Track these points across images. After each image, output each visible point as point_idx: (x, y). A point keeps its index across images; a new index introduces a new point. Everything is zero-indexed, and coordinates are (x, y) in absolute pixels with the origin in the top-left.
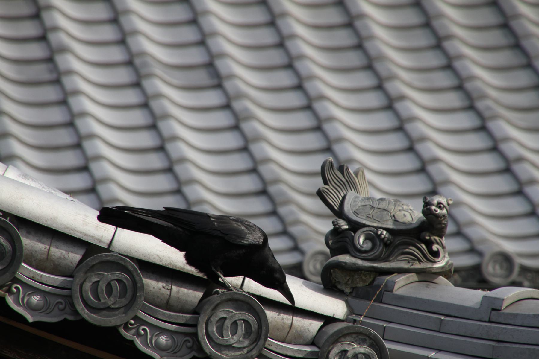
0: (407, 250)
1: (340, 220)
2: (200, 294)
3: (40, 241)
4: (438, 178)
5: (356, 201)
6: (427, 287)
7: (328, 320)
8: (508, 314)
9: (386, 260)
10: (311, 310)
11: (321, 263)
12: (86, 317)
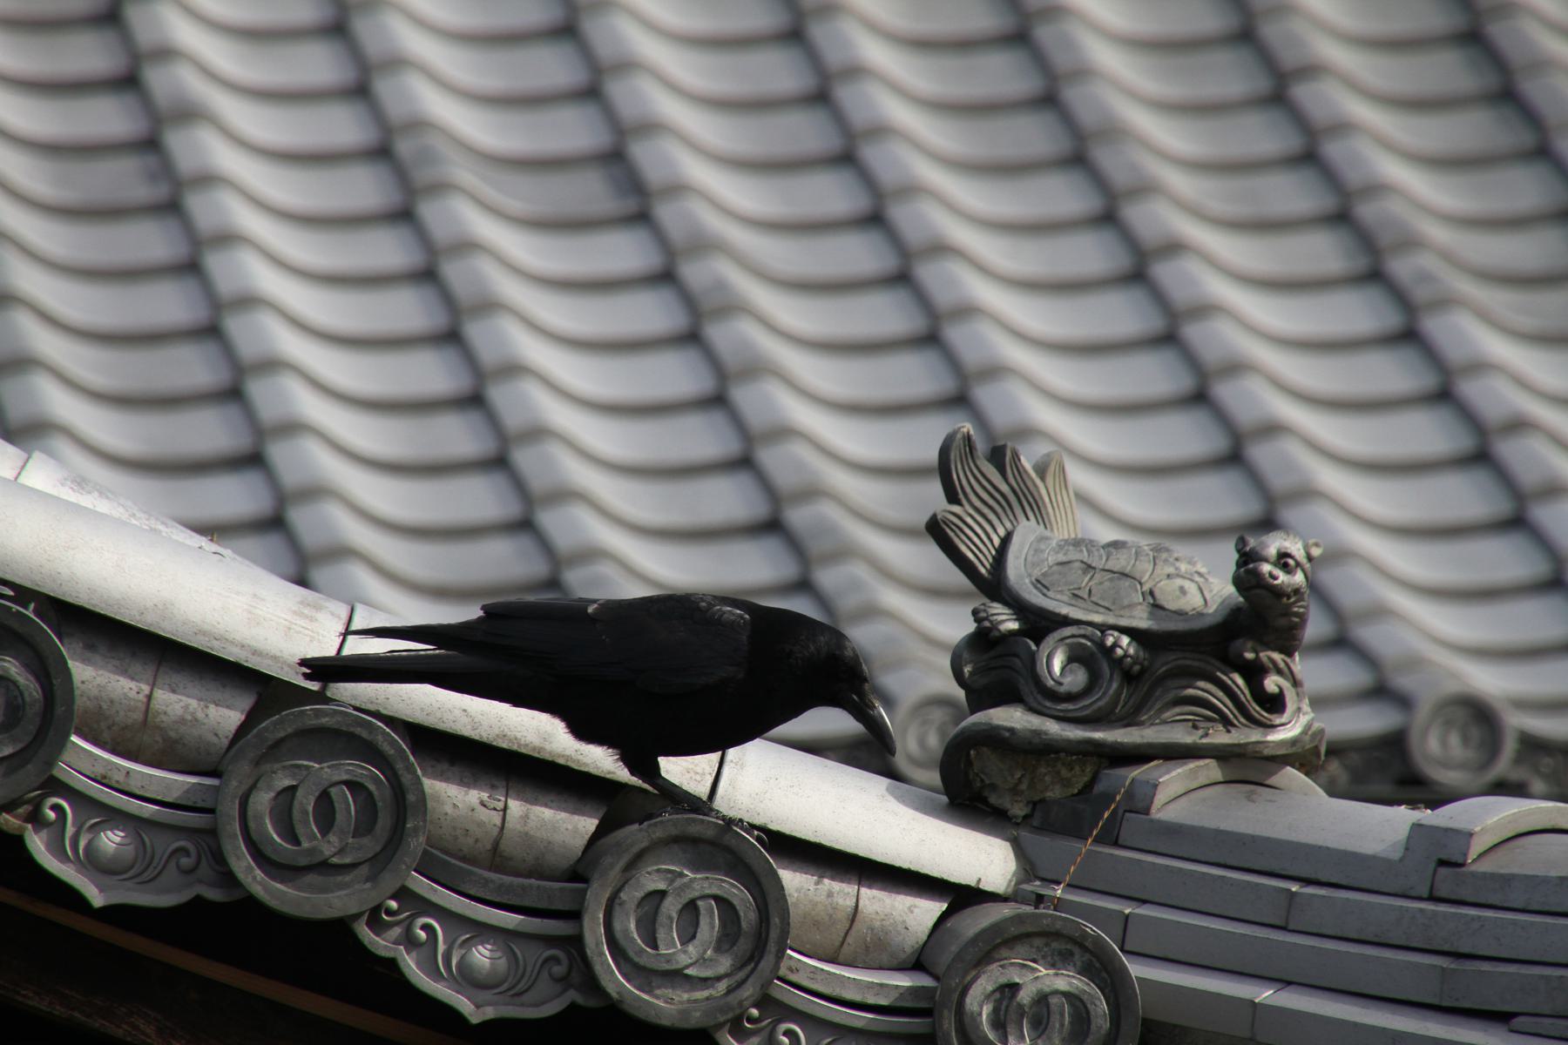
0: (1191, 691)
1: (995, 605)
2: (588, 824)
3: (124, 672)
4: (1279, 481)
7: (961, 897)
9: (1129, 720)
10: (913, 868)
11: (942, 732)
12: (257, 891)
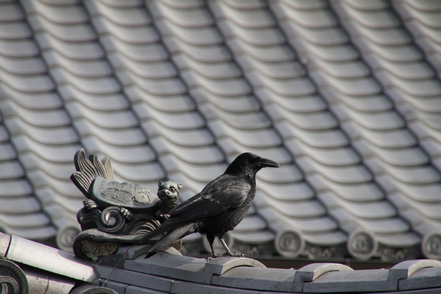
0: (145, 225)
1: (90, 200)
4: (168, 167)
5: (104, 185)
6: (161, 256)
9: (127, 233)
10: (64, 275)
11: (72, 237)
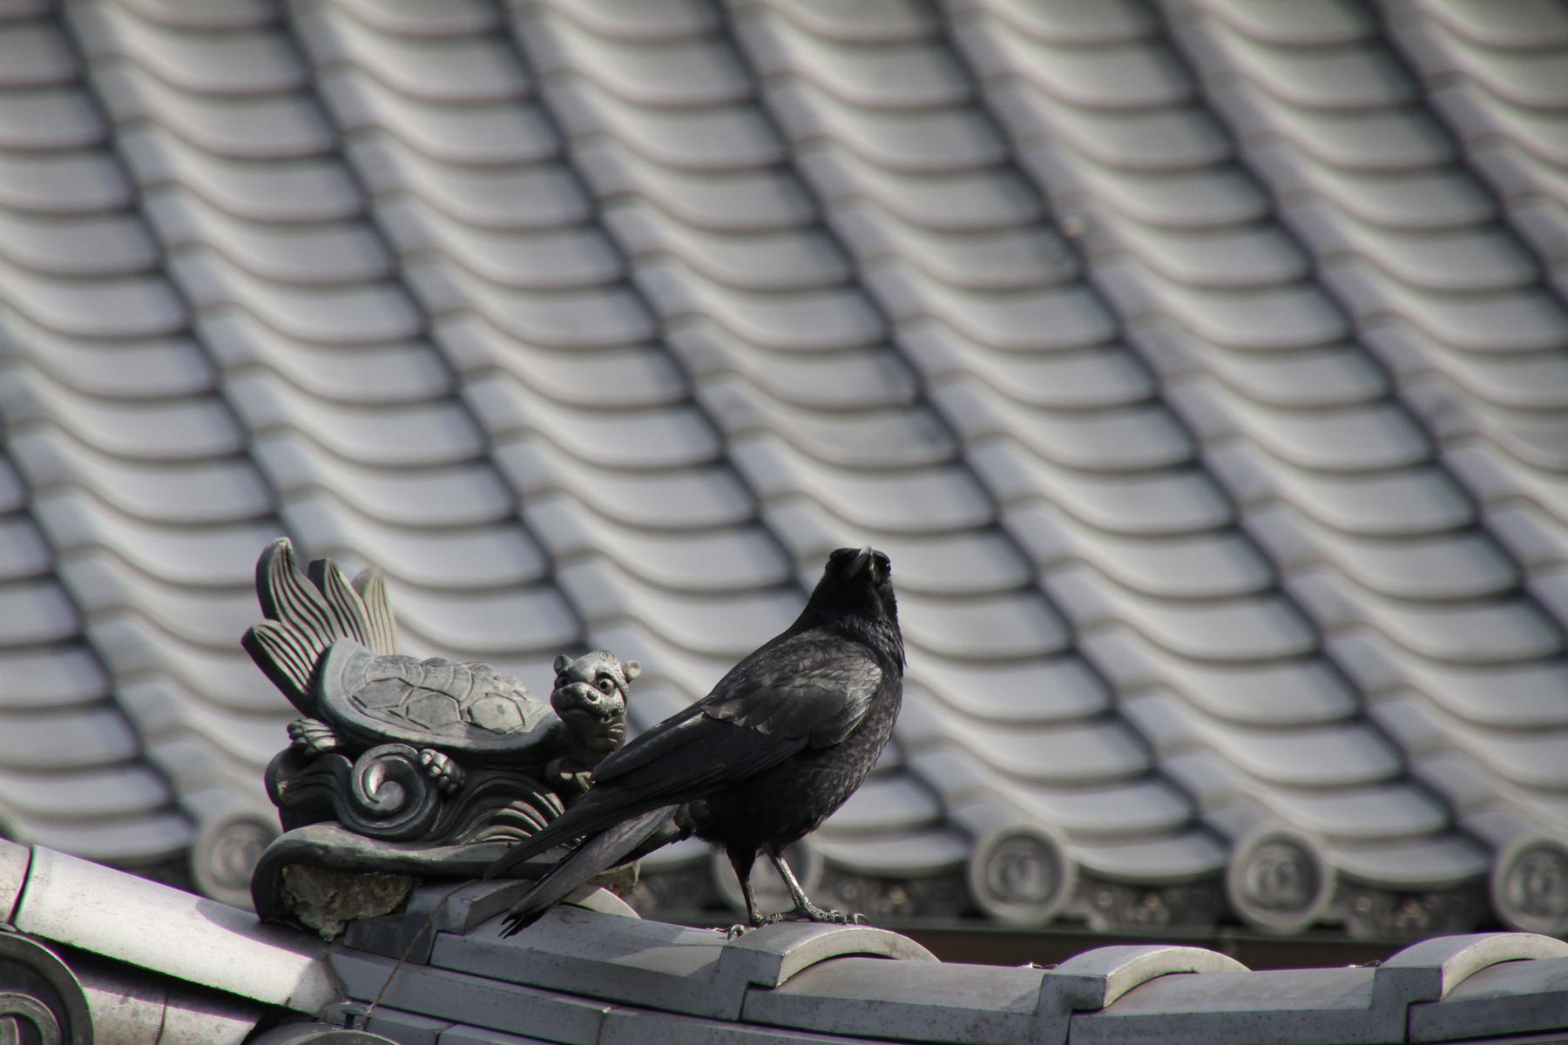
0: (506, 811)
1: (311, 721)
4: (591, 605)
5: (360, 668)
6: (563, 920)
8: (794, 998)
9: (443, 839)
11: (248, 852)
